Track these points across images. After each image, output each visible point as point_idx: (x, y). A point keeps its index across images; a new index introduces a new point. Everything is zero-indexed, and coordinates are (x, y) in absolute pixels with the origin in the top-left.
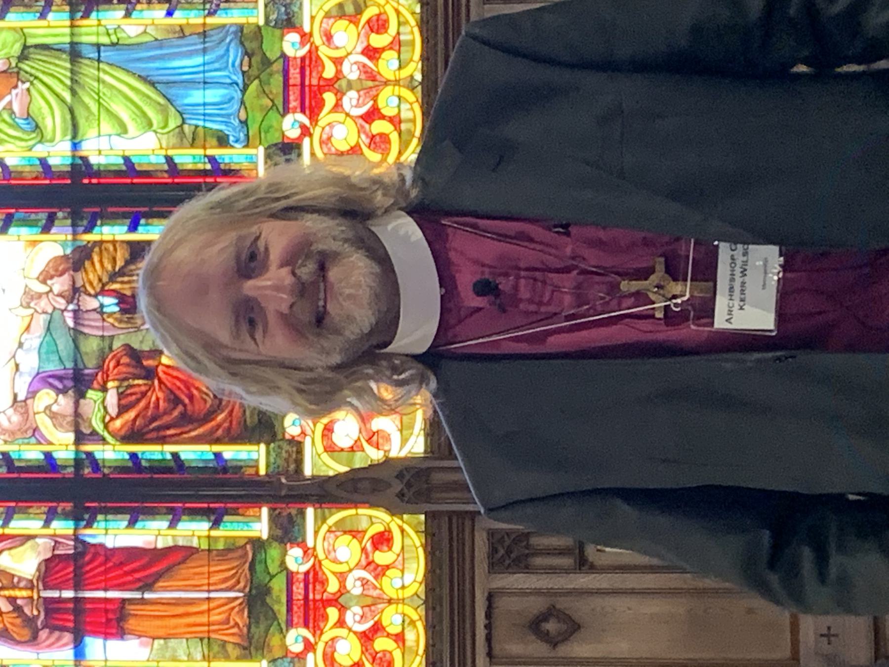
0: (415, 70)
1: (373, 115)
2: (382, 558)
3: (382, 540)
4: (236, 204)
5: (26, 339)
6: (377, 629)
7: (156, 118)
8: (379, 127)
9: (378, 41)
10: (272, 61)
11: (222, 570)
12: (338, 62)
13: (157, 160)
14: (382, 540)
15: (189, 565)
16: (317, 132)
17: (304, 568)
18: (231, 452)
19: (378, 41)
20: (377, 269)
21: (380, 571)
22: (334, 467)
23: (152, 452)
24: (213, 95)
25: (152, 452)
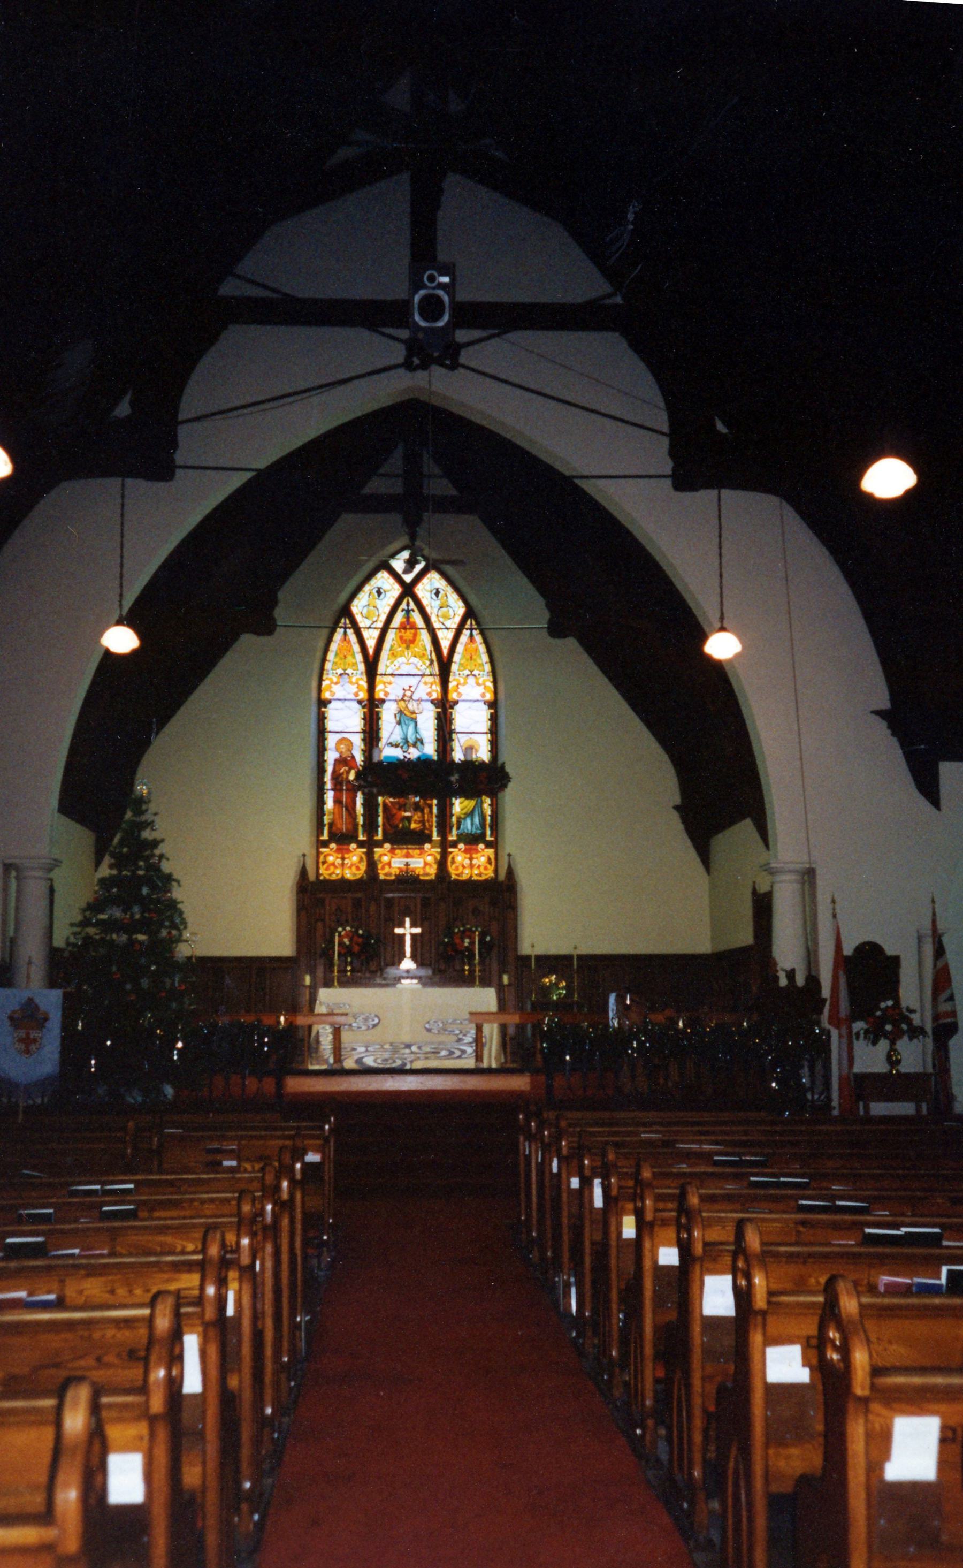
0: (475, 878)
1: (464, 867)
2: (354, 868)
3: (358, 868)
4: (97, 932)
5: (349, 693)
6: (336, 867)
7: (464, 811)
8: (461, 868)
9: (482, 869)
10: (745, 937)
11: (350, 827)
12: (477, 858)
13: (454, 812)
14: (358, 868)
15: (801, 866)
16: (460, 853)
17: (351, 849)
18: (380, 830)
19: (482, 869)
20: (160, 1300)
21: (350, 868)
22: (376, 857)
23: (380, 810)
24: (469, 826)
25: (380, 810)
